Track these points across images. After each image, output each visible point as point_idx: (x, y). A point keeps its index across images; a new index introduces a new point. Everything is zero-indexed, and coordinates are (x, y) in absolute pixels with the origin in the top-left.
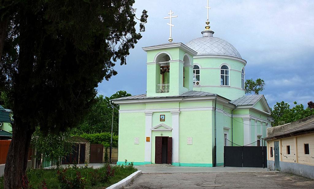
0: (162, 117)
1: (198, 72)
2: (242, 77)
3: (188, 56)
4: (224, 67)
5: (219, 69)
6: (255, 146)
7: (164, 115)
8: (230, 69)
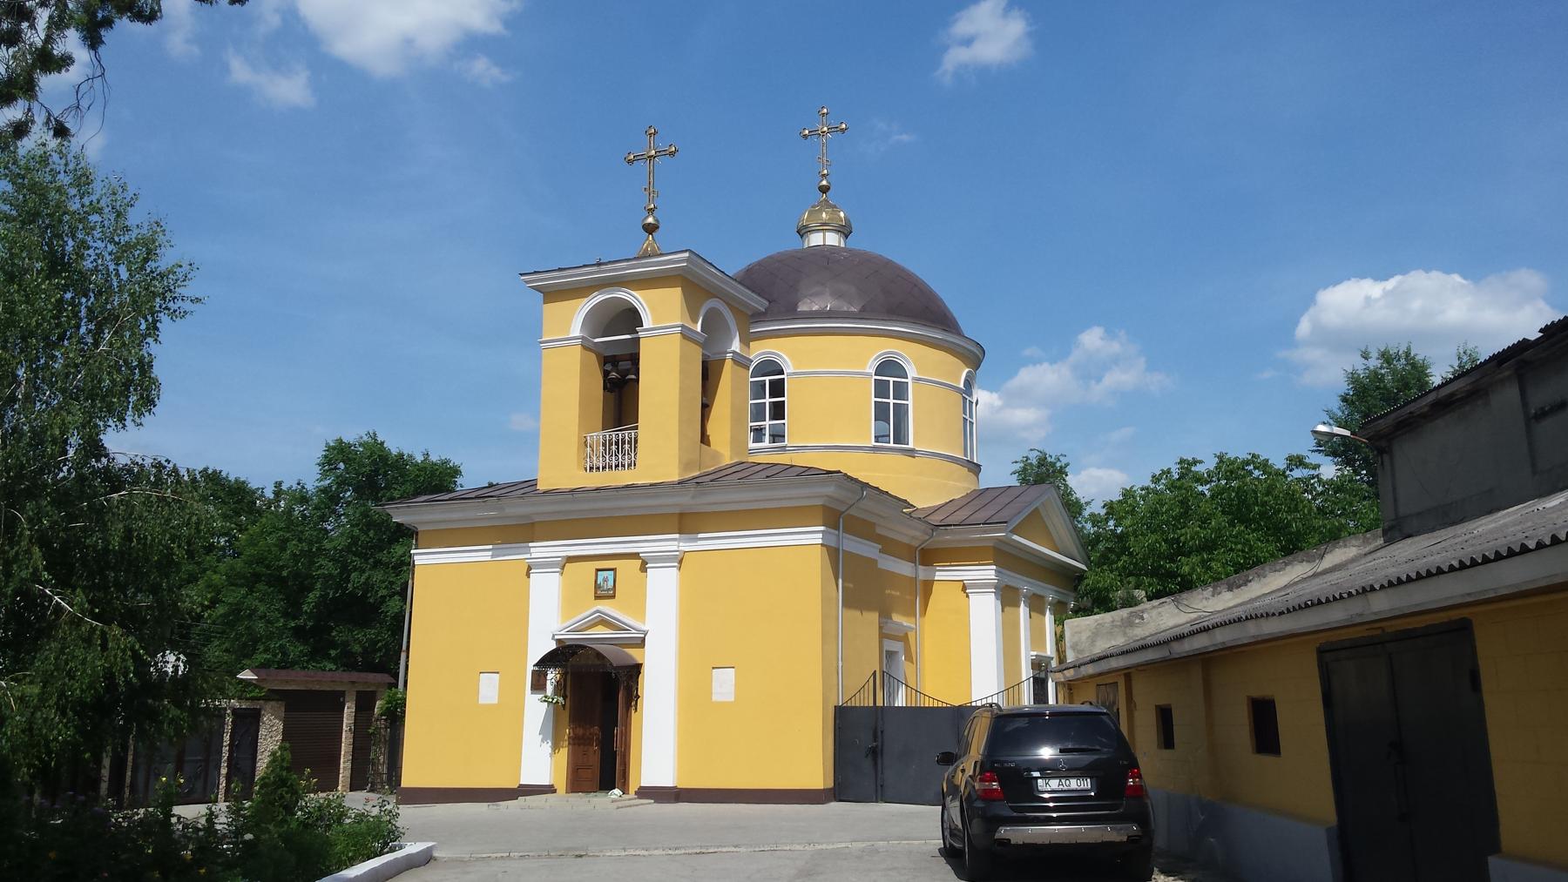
0: (605, 580)
1: (778, 389)
2: (965, 413)
4: (889, 367)
5: (869, 375)
7: (613, 570)
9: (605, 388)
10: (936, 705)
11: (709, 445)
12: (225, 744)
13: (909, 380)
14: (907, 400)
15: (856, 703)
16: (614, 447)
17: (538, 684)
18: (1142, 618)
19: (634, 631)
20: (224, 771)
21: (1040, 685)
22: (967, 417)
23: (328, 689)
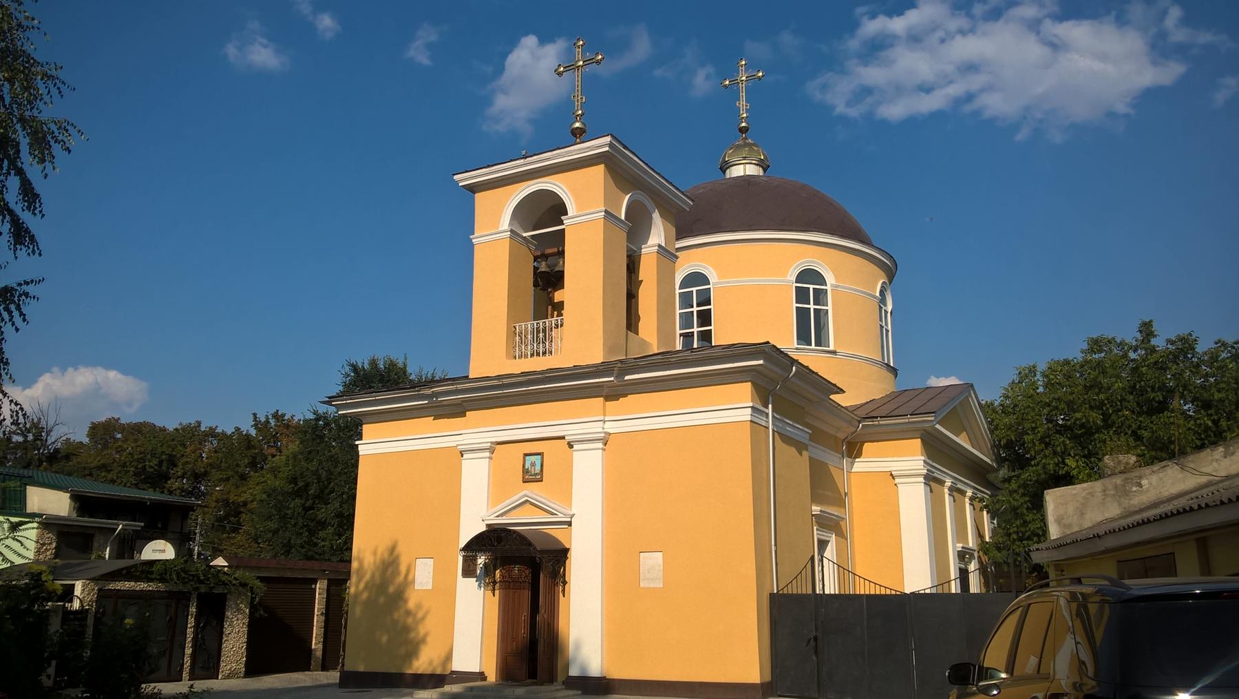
0: (533, 464)
1: (705, 299)
2: (881, 320)
3: (649, 203)
4: (810, 275)
6: (875, 595)
8: (832, 285)
9: (536, 285)
10: (883, 593)
11: (637, 333)
12: (189, 626)
13: (828, 288)
14: (827, 306)
15: (794, 590)
16: (541, 335)
17: (468, 572)
18: (1140, 485)
19: (560, 515)
20: (188, 651)
21: (964, 575)
22: (884, 324)
23: (300, 577)
